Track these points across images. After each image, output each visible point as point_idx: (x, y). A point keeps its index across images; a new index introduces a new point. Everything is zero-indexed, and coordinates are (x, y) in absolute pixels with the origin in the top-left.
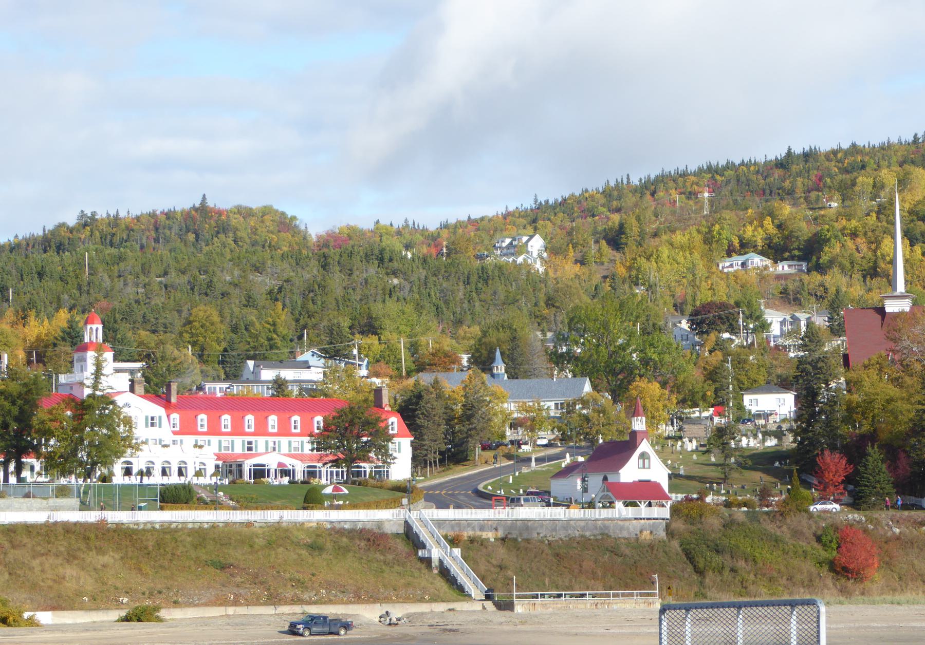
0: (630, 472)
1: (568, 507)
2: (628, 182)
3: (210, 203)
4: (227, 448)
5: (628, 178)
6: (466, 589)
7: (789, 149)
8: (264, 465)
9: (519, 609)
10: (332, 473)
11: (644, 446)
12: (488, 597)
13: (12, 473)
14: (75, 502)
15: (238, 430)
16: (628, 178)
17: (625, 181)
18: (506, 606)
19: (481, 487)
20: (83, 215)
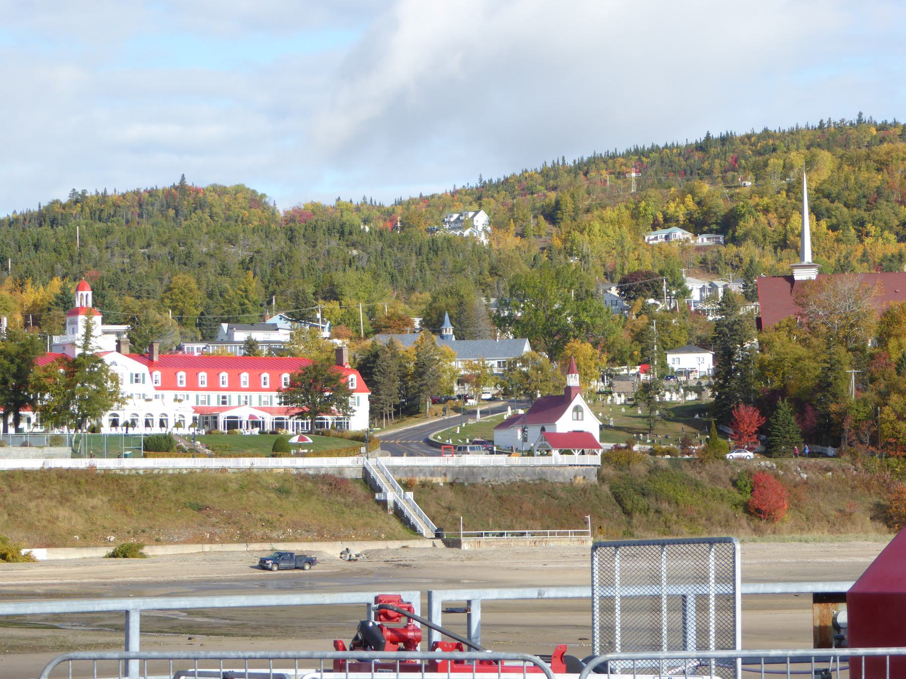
0: (565, 424)
1: (510, 454)
2: (564, 163)
3: (189, 182)
4: (203, 402)
5: (563, 160)
6: (418, 529)
7: (708, 134)
8: (237, 418)
9: (465, 546)
10: (298, 424)
11: (578, 400)
12: (438, 536)
13: (11, 424)
14: (67, 450)
15: (213, 386)
16: (563, 160)
17: (561, 163)
18: (454, 543)
19: (431, 437)
20: (74, 192)
